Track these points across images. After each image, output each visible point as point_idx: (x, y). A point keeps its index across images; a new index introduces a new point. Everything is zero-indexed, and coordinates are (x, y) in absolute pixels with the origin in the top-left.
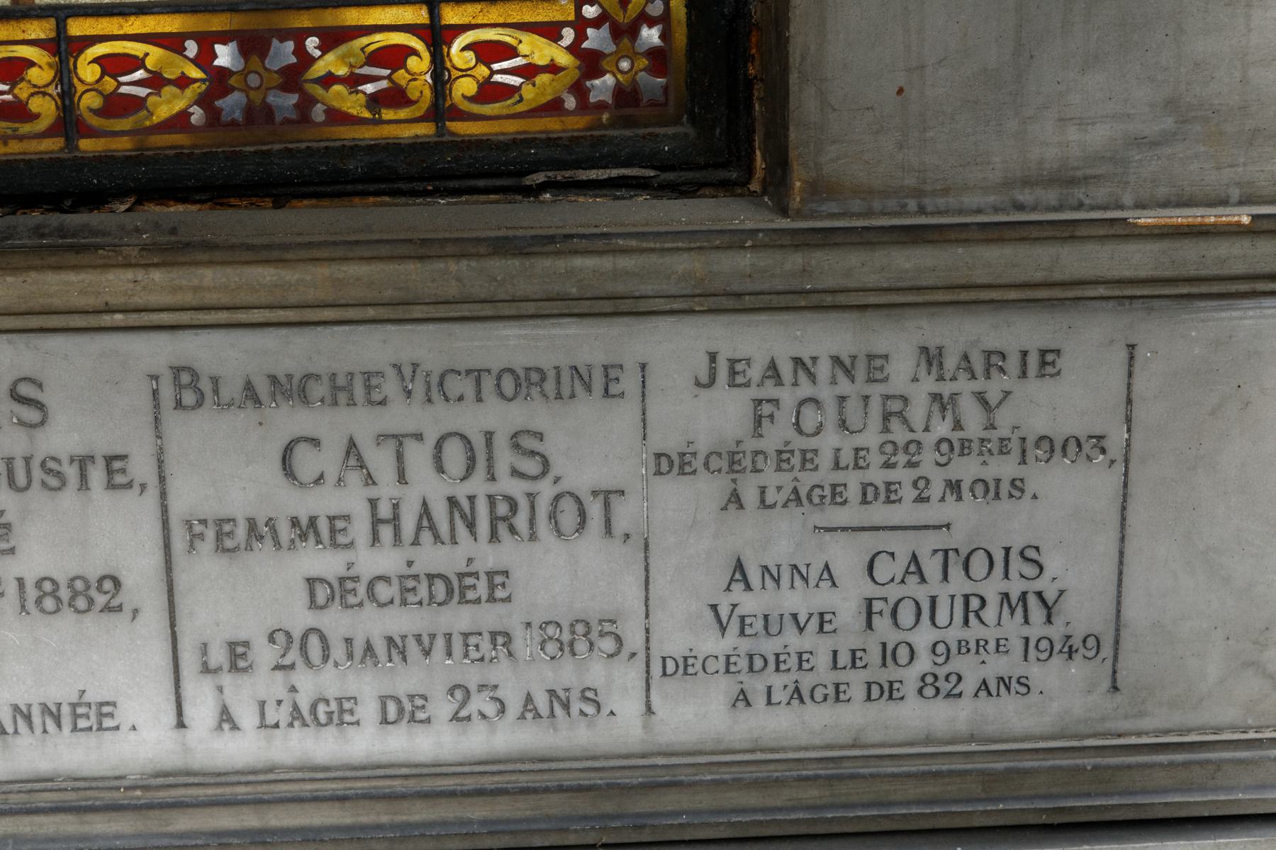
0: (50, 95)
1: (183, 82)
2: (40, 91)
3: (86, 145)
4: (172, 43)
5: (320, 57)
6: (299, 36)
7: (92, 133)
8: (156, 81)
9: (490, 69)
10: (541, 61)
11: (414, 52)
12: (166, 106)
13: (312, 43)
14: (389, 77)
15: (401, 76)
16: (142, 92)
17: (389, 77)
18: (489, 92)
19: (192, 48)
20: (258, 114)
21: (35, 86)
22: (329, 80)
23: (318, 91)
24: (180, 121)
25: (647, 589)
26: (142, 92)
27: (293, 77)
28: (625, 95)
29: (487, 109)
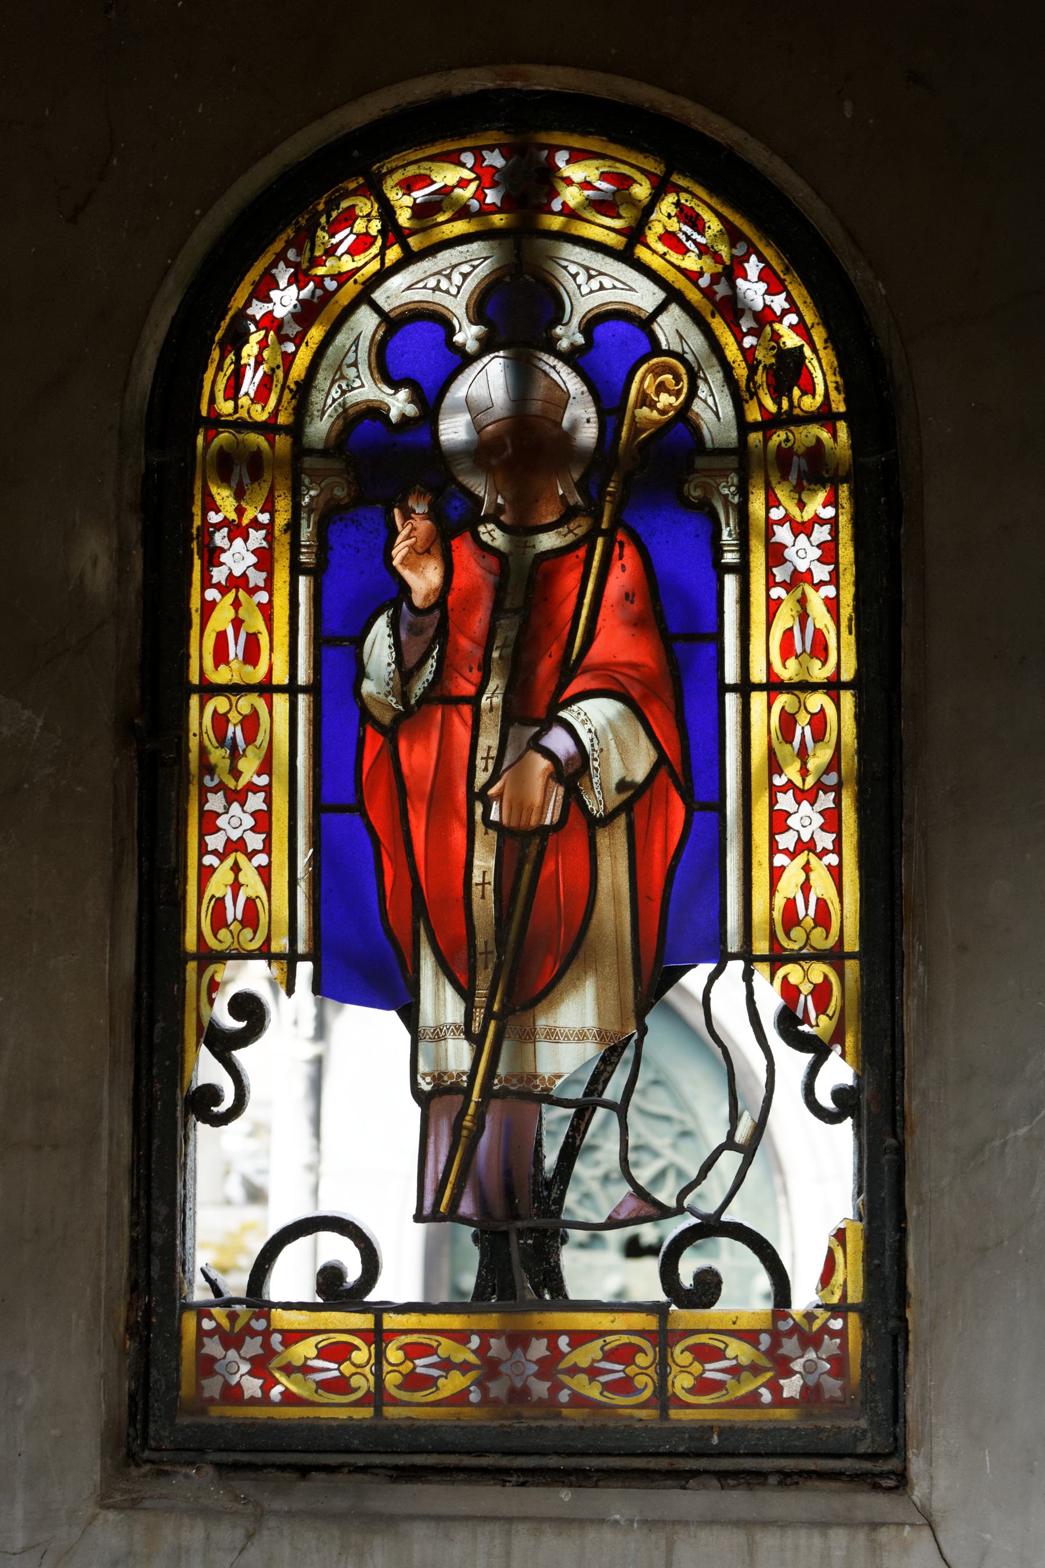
0: (677, 1365)
1: (288, 1369)
2: (684, 1369)
3: (390, 1411)
4: (460, 1337)
5: (569, 1353)
6: (553, 1336)
7: (396, 1402)
8: (446, 1365)
9: (340, 1372)
10: (744, 1361)
11: (641, 1350)
12: (452, 1384)
13: (563, 1342)
14: (623, 1371)
15: (347, 1368)
16: (435, 1372)
17: (338, 1369)
18: (704, 1386)
19: (263, 781)
20: (519, 1395)
21: (689, 1373)
22: (574, 1370)
23: (565, 1379)
24: (460, 1398)
25: (317, 1134)
26: (435, 1372)
27: (548, 1367)
28: (811, 1393)
29: (705, 1400)
